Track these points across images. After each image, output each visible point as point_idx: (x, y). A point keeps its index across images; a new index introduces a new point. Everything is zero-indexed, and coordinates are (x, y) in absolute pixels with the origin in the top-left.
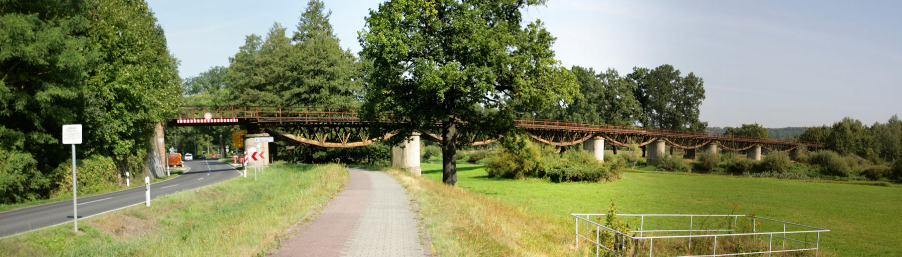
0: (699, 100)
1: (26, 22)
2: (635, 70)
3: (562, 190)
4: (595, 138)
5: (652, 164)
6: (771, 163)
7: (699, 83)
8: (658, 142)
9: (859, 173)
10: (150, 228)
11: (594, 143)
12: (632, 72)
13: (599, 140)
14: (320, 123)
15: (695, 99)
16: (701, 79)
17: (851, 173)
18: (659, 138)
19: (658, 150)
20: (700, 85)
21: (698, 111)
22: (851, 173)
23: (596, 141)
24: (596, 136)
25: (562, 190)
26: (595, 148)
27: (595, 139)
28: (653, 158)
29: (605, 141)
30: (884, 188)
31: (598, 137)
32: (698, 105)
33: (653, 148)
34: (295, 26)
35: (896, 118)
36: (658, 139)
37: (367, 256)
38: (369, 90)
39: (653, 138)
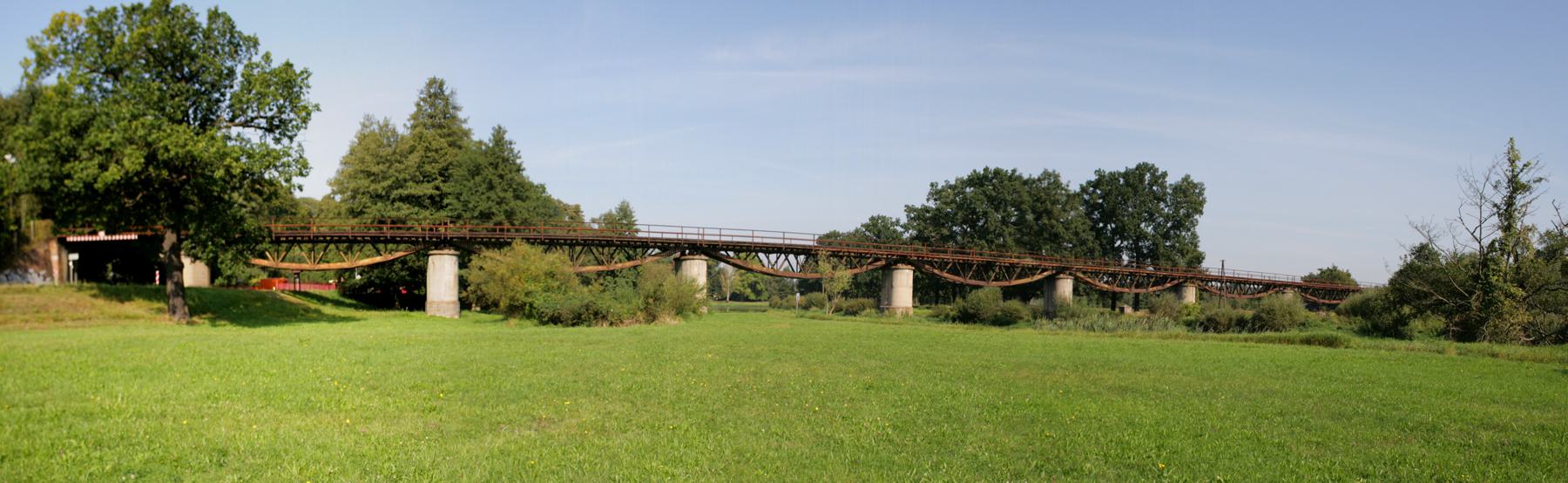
2: (1100, 175)
3: (361, 349)
4: (894, 267)
6: (1264, 315)
8: (1059, 279)
9: (1436, 330)
12: (1093, 178)
13: (1062, 280)
14: (493, 240)
15: (1188, 216)
17: (1420, 332)
18: (1061, 270)
22: (1420, 332)
23: (895, 272)
24: (896, 262)
25: (361, 349)
26: (894, 284)
30: (600, 331)
34: (1489, 167)
36: (1058, 273)
37: (1495, 482)
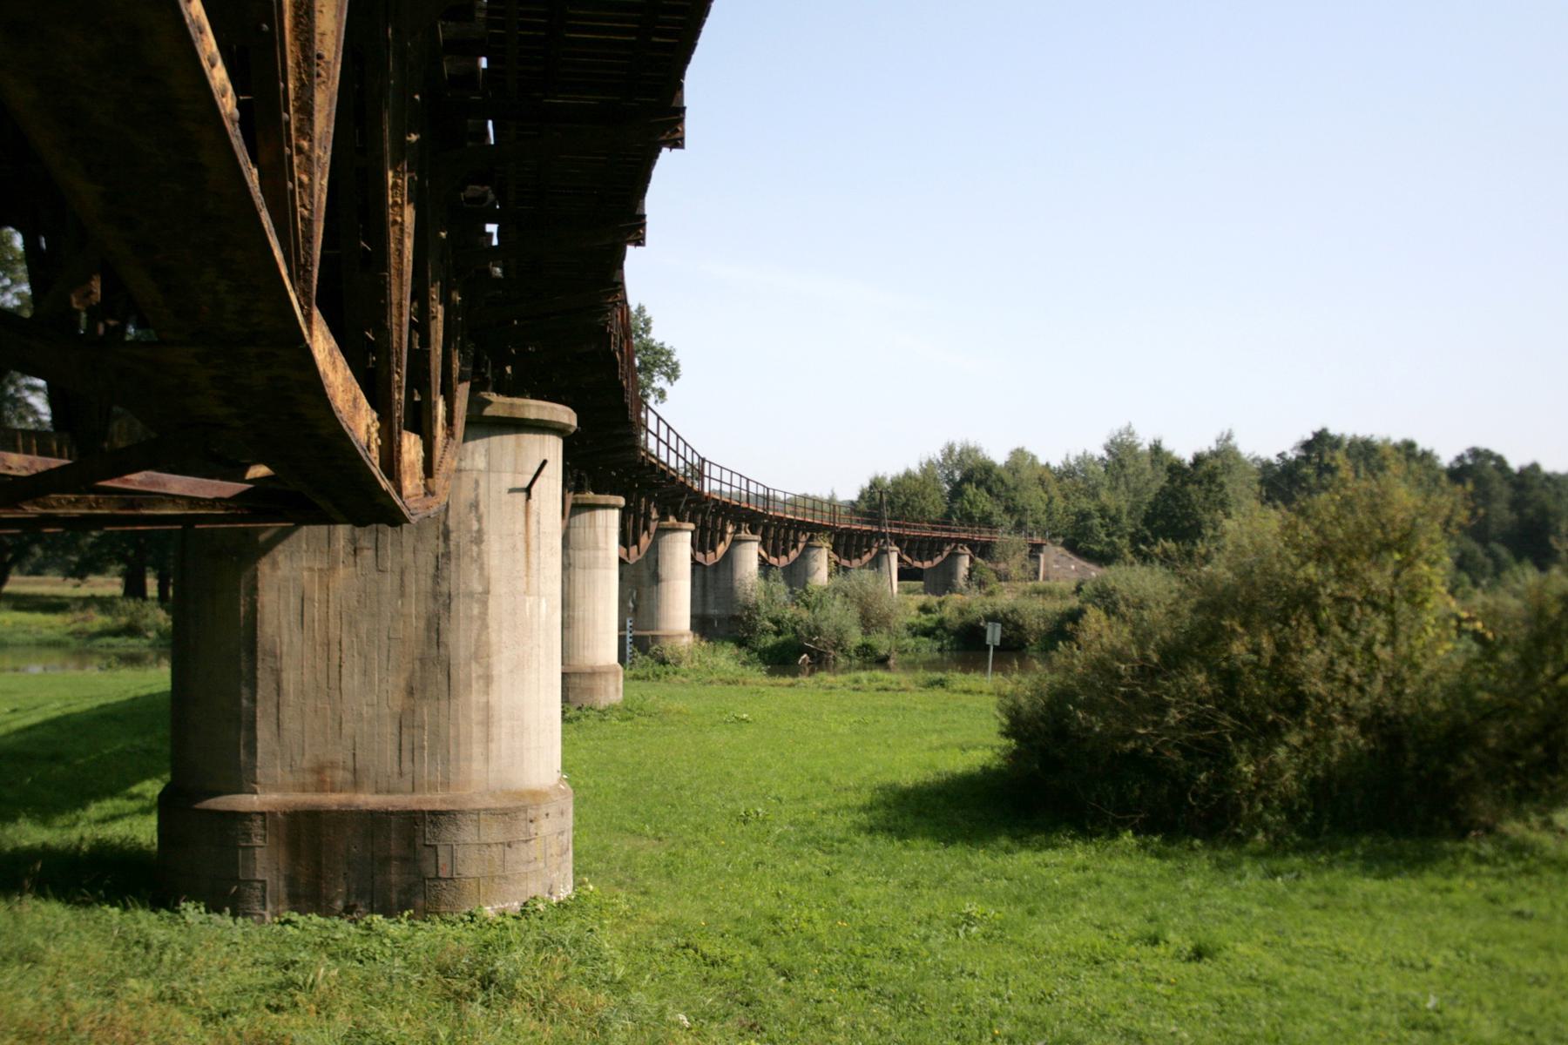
19: (738, 576)
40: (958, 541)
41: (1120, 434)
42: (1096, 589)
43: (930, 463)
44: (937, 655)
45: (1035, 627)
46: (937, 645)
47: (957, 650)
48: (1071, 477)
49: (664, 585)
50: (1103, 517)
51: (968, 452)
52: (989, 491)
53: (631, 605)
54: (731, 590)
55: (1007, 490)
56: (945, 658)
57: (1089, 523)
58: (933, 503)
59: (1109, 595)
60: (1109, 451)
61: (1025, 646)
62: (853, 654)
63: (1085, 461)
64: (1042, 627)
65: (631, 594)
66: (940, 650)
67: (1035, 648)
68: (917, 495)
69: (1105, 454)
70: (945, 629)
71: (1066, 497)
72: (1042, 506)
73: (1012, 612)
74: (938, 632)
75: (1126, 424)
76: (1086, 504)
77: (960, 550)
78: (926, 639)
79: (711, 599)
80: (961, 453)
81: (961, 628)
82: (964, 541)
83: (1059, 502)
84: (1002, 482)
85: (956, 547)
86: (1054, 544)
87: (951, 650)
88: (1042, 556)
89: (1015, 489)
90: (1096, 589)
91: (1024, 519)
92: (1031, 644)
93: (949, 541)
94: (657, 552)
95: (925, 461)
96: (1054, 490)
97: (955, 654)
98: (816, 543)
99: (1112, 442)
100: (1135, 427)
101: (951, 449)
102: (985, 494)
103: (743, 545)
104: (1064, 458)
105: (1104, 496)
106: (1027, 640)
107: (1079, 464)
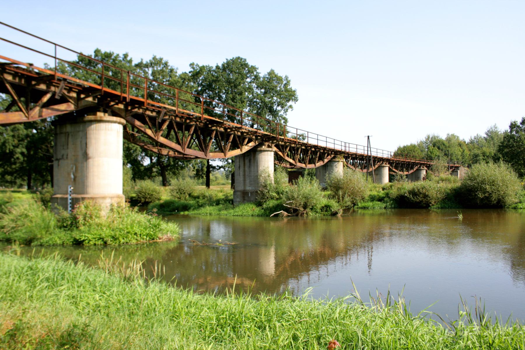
0: (289, 104)
1: (96, 318)
4: (91, 117)
5: (249, 201)
7: (285, 82)
8: (261, 151)
10: (59, 293)
11: (85, 136)
13: (103, 125)
16: (287, 78)
19: (261, 168)
20: (286, 85)
21: (286, 121)
23: (94, 126)
26: (91, 151)
27: (91, 122)
28: (248, 188)
29: (127, 137)
31: (100, 114)
32: (286, 111)
33: (250, 167)
35: (496, 128)
38: (43, 326)
39: (250, 141)
40: (421, 164)
41: (491, 128)
42: (469, 176)
43: (421, 142)
44: (384, 211)
45: (435, 195)
46: (384, 205)
47: (394, 208)
48: (474, 143)
49: (90, 161)
50: (484, 156)
51: (434, 137)
52: (439, 148)
53: (72, 176)
54: (256, 178)
55: (446, 147)
56: (388, 212)
57: (478, 158)
58: (418, 153)
59: (475, 179)
60: (487, 134)
61: (430, 206)
62: (319, 210)
63: (477, 138)
64: (439, 196)
65: (72, 169)
66: (385, 208)
67: (435, 207)
68: (411, 151)
69: (485, 136)
70: (389, 198)
71: (470, 150)
72: (460, 153)
73: (423, 189)
74: (385, 199)
75: (494, 124)
76: (476, 151)
77: (422, 168)
78: (379, 202)
79: (247, 181)
80: (432, 138)
81: (397, 197)
82: (424, 164)
83: (467, 152)
84: (444, 145)
85: (420, 167)
86: (464, 167)
87: (391, 208)
88: (459, 171)
89: (449, 147)
90: (469, 176)
91: (452, 158)
92: (433, 205)
93: (417, 164)
94: (86, 138)
95: (419, 141)
96: (465, 148)
97: (393, 210)
98: (337, 160)
99: (488, 131)
100: (497, 125)
101: (429, 137)
102: (437, 149)
103: (263, 153)
104: (470, 138)
105: (484, 149)
106: (431, 203)
107: (475, 138)
